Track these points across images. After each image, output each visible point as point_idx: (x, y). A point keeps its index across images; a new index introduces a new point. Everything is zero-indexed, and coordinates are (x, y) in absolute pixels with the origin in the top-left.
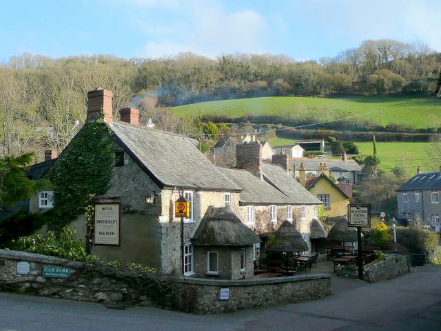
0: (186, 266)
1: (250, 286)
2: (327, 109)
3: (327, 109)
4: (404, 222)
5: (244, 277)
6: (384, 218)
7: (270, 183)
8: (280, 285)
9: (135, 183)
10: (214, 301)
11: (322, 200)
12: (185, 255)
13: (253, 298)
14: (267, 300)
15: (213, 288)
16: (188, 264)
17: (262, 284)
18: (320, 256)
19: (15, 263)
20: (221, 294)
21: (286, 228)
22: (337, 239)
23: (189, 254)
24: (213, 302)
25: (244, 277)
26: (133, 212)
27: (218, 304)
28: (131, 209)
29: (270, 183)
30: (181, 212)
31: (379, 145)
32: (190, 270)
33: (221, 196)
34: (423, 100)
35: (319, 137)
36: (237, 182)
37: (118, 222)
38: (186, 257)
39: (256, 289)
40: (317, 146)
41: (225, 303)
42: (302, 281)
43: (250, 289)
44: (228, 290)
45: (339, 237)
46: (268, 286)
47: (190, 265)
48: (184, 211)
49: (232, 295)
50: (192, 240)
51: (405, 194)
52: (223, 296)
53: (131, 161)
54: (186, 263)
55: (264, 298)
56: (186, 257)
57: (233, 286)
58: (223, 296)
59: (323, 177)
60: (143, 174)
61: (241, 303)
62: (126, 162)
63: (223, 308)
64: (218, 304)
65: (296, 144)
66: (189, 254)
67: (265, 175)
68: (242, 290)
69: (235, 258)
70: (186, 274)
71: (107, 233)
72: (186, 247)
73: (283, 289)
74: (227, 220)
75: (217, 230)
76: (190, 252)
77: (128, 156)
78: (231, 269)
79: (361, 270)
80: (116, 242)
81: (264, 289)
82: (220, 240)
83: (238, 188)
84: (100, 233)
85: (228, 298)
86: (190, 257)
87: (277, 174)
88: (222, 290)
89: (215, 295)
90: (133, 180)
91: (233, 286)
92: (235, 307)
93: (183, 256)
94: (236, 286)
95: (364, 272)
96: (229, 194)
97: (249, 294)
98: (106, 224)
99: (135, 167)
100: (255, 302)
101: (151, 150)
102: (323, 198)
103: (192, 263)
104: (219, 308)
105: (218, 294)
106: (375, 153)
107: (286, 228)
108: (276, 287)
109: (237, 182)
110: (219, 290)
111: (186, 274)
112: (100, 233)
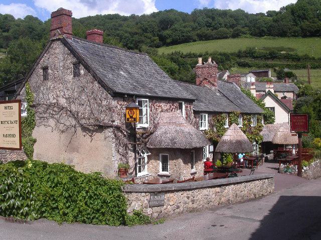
2: (169, 186)
3: (169, 186)
5: (194, 178)
13: (193, 201)
15: (143, 194)
25: (194, 178)
31: (313, 72)
35: (268, 66)
39: (196, 192)
42: (184, 190)
46: (208, 190)
55: (205, 201)
62: (82, 72)
79: (300, 168)
81: (205, 191)
84: (14, 136)
95: (303, 170)
97: (188, 198)
100: (195, 206)
108: (218, 189)
111: (139, 174)
112: (14, 136)
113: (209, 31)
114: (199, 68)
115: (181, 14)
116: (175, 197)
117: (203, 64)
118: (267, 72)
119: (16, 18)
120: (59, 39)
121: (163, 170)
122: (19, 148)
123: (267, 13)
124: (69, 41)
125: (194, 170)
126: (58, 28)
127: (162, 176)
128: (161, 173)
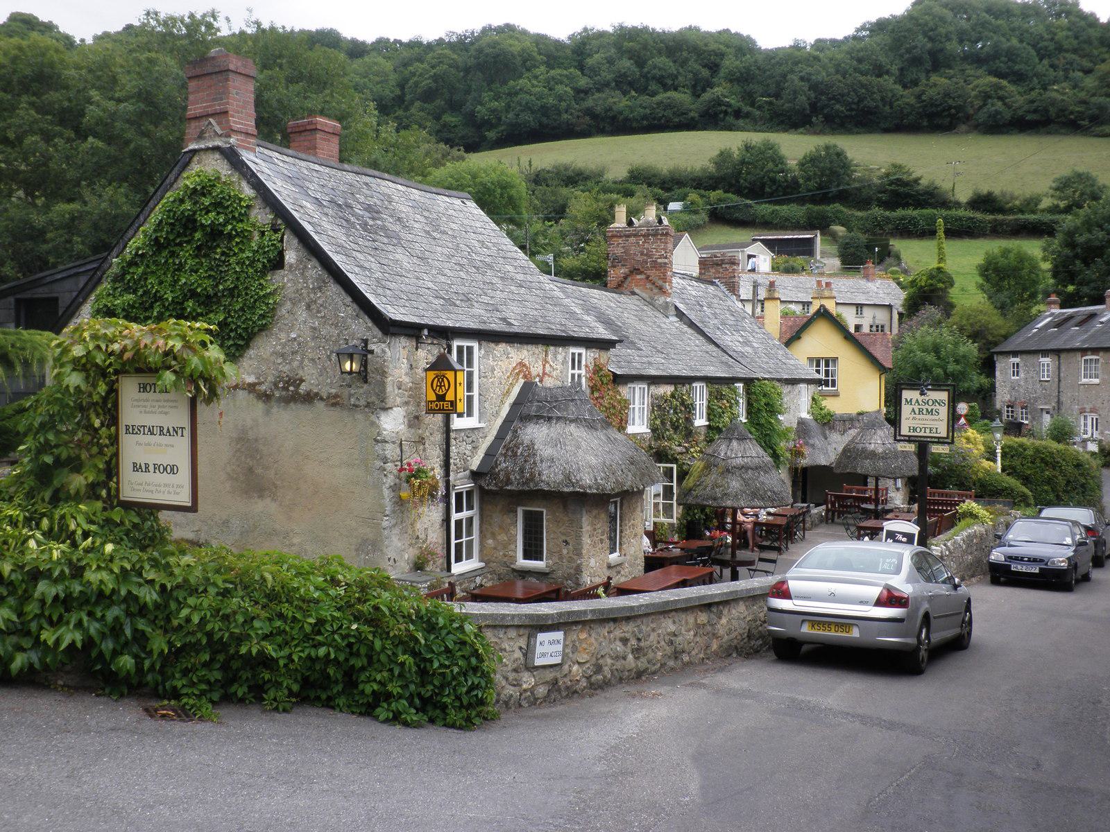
0: (459, 546)
1: (628, 619)
4: (1014, 428)
6: (966, 416)
7: (692, 325)
8: (714, 609)
9: (312, 317)
10: (515, 670)
11: (818, 372)
12: (455, 516)
13: (637, 651)
14: (676, 655)
15: (512, 633)
16: (464, 539)
17: (665, 611)
18: (815, 511)
19: (453, 435)
20: (539, 650)
21: (735, 443)
22: (859, 470)
23: (464, 514)
24: (512, 676)
26: (309, 398)
27: (528, 681)
28: (303, 388)
29: (692, 325)
30: (441, 398)
32: (469, 556)
33: (560, 357)
34: (1056, 133)
36: (608, 323)
37: (187, 433)
38: (459, 523)
40: (806, 248)
41: (549, 675)
42: (615, 620)
43: (628, 629)
44: (559, 635)
45: (864, 467)
47: (470, 544)
48: (450, 396)
49: (570, 649)
50: (475, 475)
51: (1017, 360)
52: (543, 655)
53: (303, 253)
54: (458, 536)
55: (669, 650)
56: (459, 523)
57: (576, 623)
58: (543, 655)
59: (823, 314)
60: (334, 289)
61: (599, 669)
62: (290, 257)
63: (542, 691)
64: (528, 681)
65: (755, 241)
66: (464, 514)
67: (682, 307)
68: (605, 631)
69: (590, 528)
70: (457, 568)
71: (156, 467)
72: (459, 496)
73: (724, 621)
74: (572, 421)
75: (545, 451)
76: (470, 507)
77: (295, 241)
78: (580, 555)
80: (184, 498)
81: (669, 625)
82: (550, 476)
83: (602, 332)
84: (173, 469)
85: (558, 660)
86: (470, 520)
87: (710, 306)
88: (542, 637)
89: (518, 654)
90: (308, 307)
91: (576, 623)
92: (584, 683)
93: (447, 520)
94: (584, 623)
96: (582, 351)
97: (625, 641)
98: (149, 438)
99: (314, 270)
100: (642, 664)
101: (365, 226)
102: (823, 368)
103: (475, 536)
104: (532, 690)
105: (528, 652)
106: (941, 260)
107: (735, 443)
108: (703, 617)
109: (608, 323)
110: (531, 637)
111: (457, 568)
112: (173, 469)
113: (620, 102)
114: (619, 235)
115: (540, 40)
116: (593, 640)
117: (630, 223)
118: (810, 242)
119: (611, 30)
120: (216, 149)
121: (528, 555)
122: (190, 504)
123: (569, 38)
124: (246, 156)
125: (614, 557)
126: (212, 115)
127: (524, 573)
128: (522, 563)
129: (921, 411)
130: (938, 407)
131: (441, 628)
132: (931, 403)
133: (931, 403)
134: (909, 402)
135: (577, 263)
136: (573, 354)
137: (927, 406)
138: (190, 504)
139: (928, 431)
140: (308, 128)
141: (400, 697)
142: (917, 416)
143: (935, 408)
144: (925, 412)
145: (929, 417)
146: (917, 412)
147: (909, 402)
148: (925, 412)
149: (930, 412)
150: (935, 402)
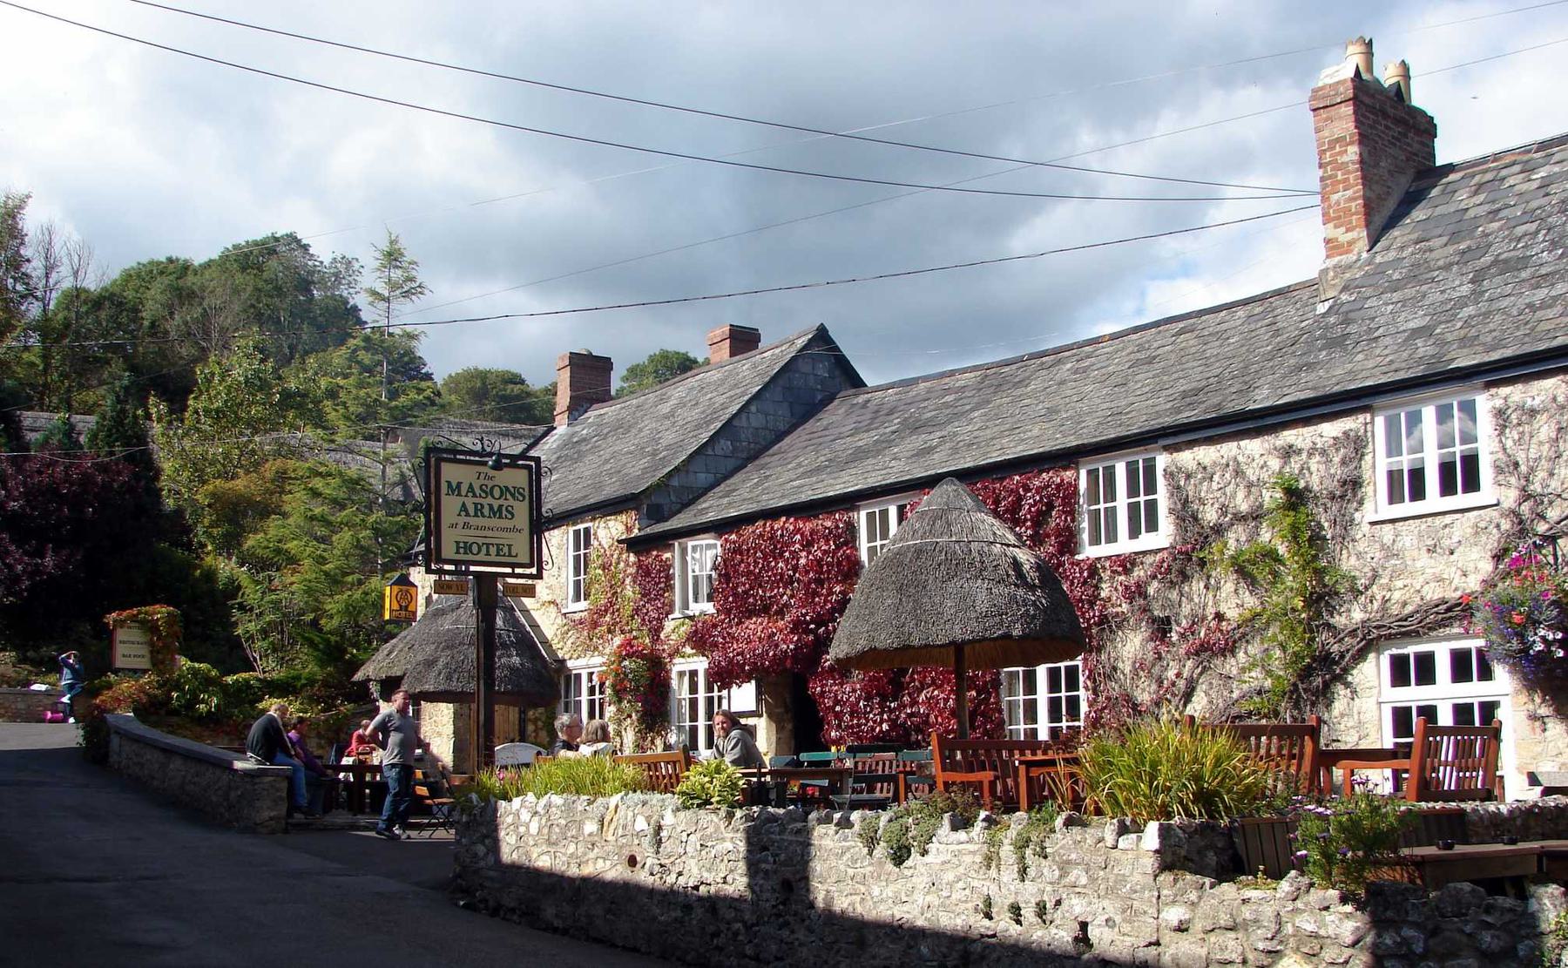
122: (442, 464)
129: (479, 511)
130: (511, 501)
131: (1329, 626)
132: (497, 493)
133: (497, 493)
134: (455, 489)
135: (529, 732)
136: (577, 533)
137: (490, 500)
138: (442, 464)
139: (493, 550)
140: (917, 399)
141: (358, 362)
142: (473, 521)
143: (506, 503)
144: (486, 511)
145: (495, 522)
146: (472, 512)
147: (455, 489)
148: (486, 511)
149: (496, 513)
150: (505, 491)
